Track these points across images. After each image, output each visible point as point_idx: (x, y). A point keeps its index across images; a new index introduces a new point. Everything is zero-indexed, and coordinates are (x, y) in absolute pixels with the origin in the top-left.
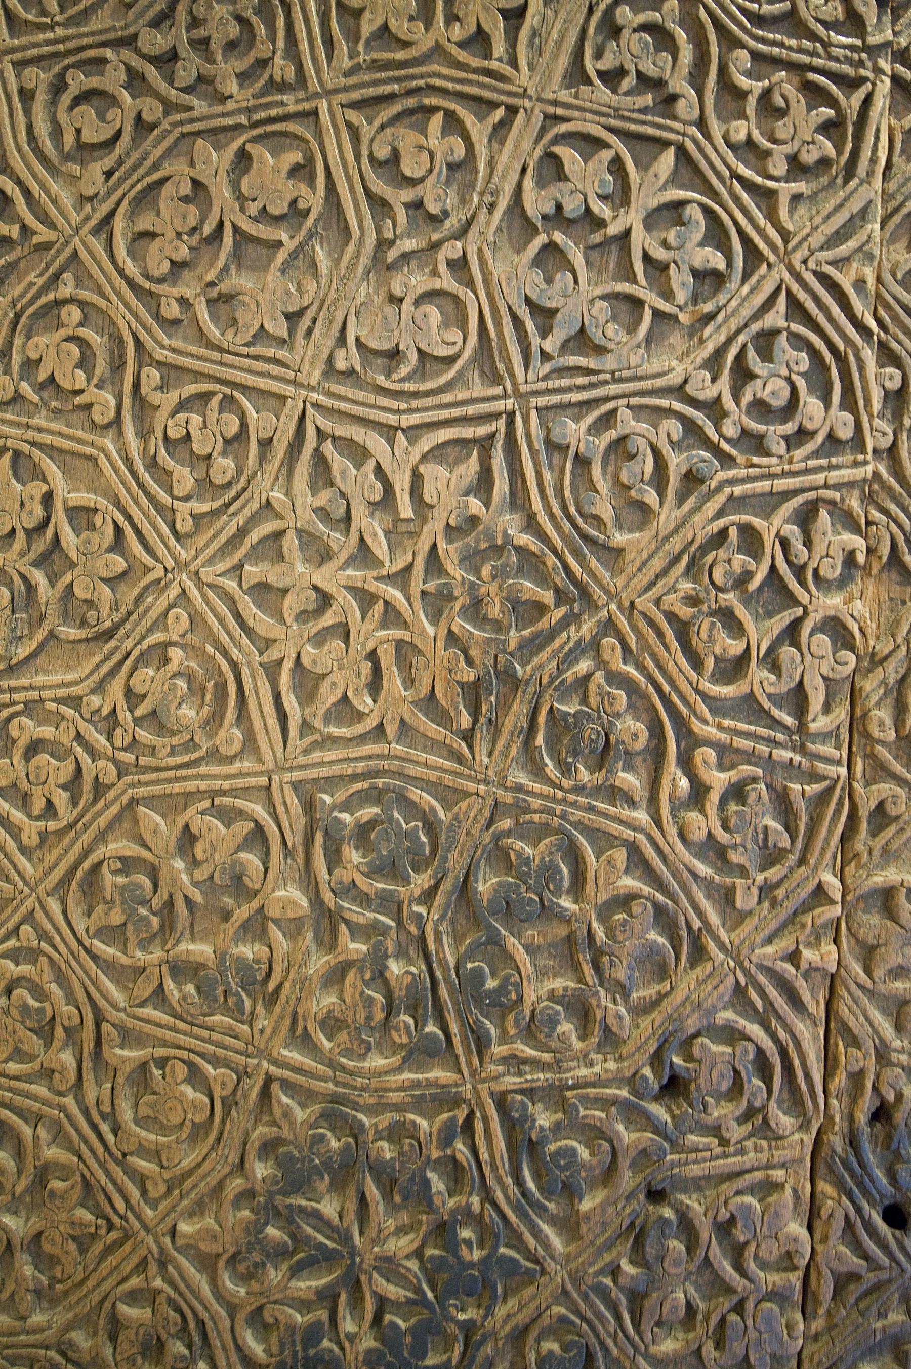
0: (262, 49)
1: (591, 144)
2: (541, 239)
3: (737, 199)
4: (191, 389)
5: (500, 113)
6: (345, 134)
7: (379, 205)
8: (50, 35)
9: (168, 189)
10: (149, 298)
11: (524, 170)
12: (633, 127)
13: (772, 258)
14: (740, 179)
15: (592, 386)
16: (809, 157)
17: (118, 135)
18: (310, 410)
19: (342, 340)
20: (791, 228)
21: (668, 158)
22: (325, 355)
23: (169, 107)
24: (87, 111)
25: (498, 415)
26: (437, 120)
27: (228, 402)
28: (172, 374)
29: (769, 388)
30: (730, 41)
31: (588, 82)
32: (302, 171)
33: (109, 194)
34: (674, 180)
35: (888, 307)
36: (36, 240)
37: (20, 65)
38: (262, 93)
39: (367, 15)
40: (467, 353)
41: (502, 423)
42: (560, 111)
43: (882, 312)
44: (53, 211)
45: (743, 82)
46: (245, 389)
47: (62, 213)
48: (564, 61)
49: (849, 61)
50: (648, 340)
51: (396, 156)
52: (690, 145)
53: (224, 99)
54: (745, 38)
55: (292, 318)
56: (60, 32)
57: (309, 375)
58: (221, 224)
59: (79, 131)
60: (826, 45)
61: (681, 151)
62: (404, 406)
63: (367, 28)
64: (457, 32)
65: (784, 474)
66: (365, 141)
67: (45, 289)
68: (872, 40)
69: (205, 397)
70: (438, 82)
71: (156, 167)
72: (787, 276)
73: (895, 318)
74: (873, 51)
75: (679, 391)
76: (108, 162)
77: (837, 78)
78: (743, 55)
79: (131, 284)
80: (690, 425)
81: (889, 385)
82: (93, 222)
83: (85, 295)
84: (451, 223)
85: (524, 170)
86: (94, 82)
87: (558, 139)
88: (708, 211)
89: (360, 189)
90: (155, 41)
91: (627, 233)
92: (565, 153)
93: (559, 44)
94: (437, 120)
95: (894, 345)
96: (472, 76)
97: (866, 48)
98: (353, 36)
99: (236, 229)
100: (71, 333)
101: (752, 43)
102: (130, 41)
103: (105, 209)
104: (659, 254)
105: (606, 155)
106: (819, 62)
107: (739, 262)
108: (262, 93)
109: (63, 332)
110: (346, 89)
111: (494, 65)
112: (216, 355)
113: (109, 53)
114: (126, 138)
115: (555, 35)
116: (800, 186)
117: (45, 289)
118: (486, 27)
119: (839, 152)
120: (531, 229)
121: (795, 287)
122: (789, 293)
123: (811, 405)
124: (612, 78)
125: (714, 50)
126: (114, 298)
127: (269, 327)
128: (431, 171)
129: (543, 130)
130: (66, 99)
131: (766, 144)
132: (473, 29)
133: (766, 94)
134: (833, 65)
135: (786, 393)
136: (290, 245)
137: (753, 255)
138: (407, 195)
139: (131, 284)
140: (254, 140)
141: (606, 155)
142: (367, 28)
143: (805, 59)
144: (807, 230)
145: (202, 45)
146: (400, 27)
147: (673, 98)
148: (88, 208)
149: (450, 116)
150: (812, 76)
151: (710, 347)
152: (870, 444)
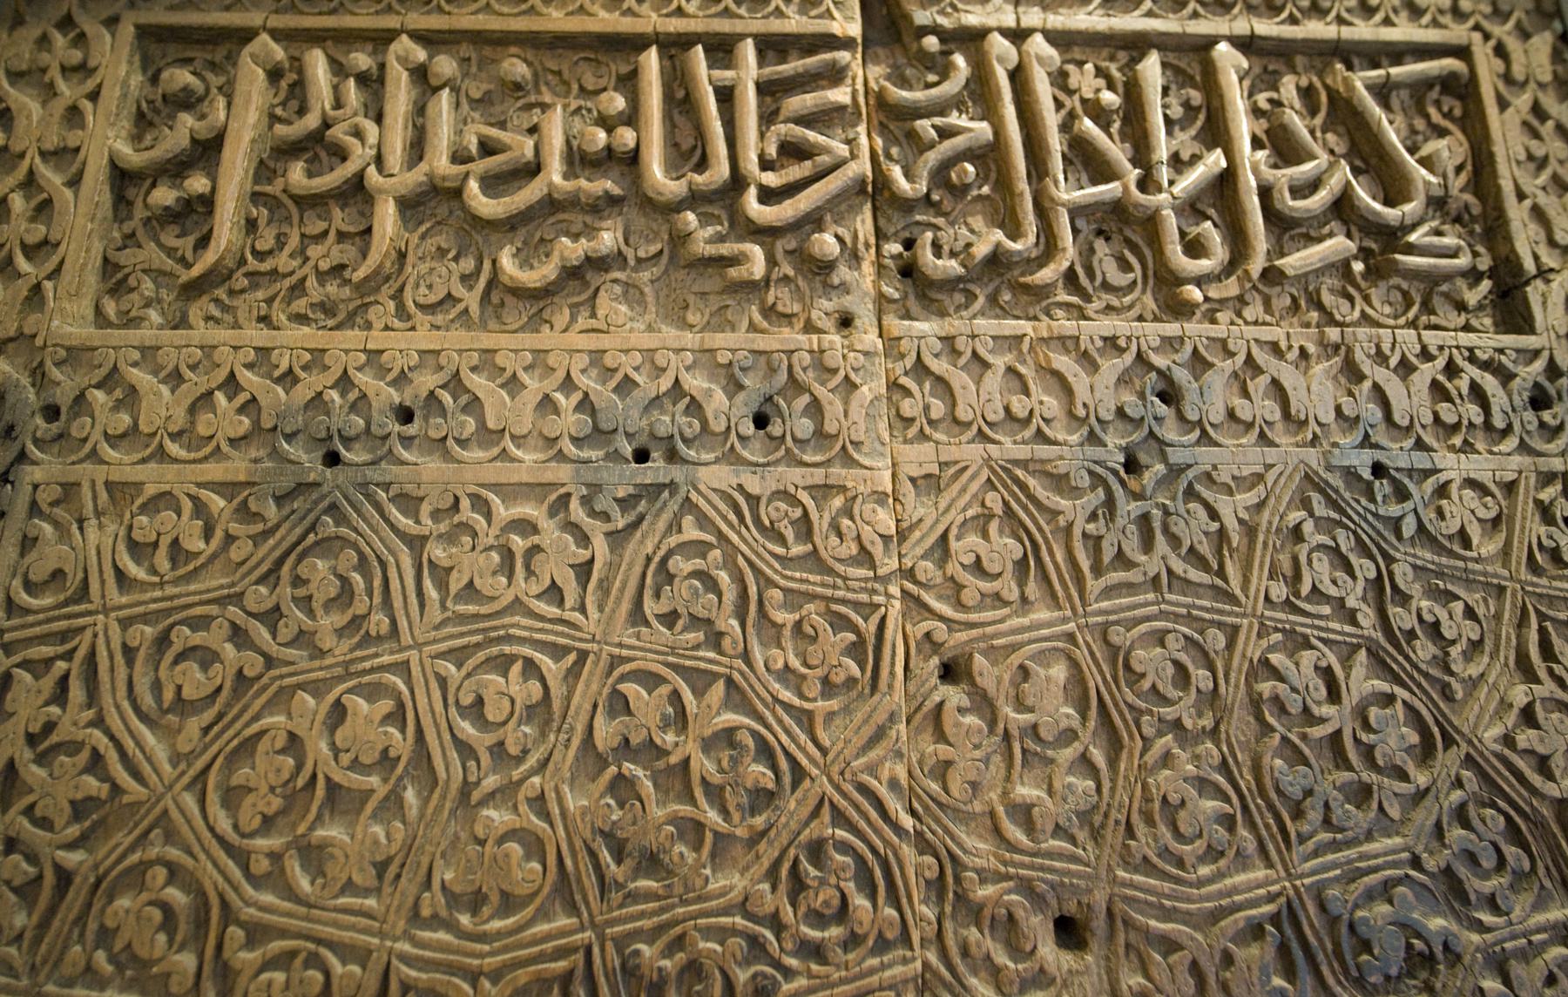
0: (360, 607)
1: (651, 680)
2: (613, 769)
3: (780, 722)
4: (277, 946)
5: (572, 657)
6: (434, 685)
7: (466, 750)
8: (158, 594)
9: (263, 746)
10: (242, 858)
11: (595, 706)
12: (688, 663)
13: (815, 771)
14: (782, 703)
15: (663, 910)
16: (839, 678)
17: (219, 689)
18: (395, 962)
19: (428, 884)
20: (827, 743)
21: (720, 687)
22: (411, 900)
23: (270, 662)
24: (192, 667)
25: (576, 950)
26: (517, 668)
27: (314, 961)
28: (256, 934)
29: (821, 898)
30: (766, 582)
31: (647, 624)
32: (397, 717)
33: (205, 749)
34: (727, 704)
35: (919, 798)
36: (126, 799)
37: (125, 623)
38: (359, 646)
39: (454, 574)
40: (546, 890)
41: (579, 957)
42: (625, 652)
43: (916, 805)
44: (146, 769)
45: (780, 616)
46: (330, 944)
47: (156, 770)
48: (626, 606)
49: (865, 590)
50: (713, 855)
51: (480, 701)
52: (736, 676)
53: (322, 653)
54: (777, 578)
55: (381, 867)
56: (170, 590)
57: (394, 926)
58: (314, 776)
59: (179, 688)
60: (845, 579)
61: (730, 682)
62: (487, 948)
63: (456, 584)
64: (535, 589)
65: (842, 981)
66: (451, 691)
67: (132, 849)
68: (880, 572)
69: (293, 954)
70: (518, 632)
71: (256, 718)
72: (830, 789)
73: (926, 808)
74: (885, 580)
75: (743, 906)
76: (209, 716)
77: (856, 605)
78: (777, 594)
79: (221, 840)
80: (755, 942)
81: (928, 874)
82: (186, 779)
83: (174, 853)
84: (532, 761)
85: (595, 706)
86: (198, 638)
87: (623, 678)
88: (755, 734)
89: (447, 737)
90: (259, 597)
91: (687, 761)
92: (629, 688)
93: (622, 590)
94: (517, 668)
95: (929, 835)
96: (548, 626)
97: (876, 578)
98: (442, 586)
99: (328, 779)
100: (153, 897)
101: (782, 582)
102: (237, 599)
103: (200, 764)
104: (717, 779)
105: (664, 690)
106: (840, 593)
107: (787, 779)
108: (359, 646)
109: (145, 896)
110: (435, 641)
111: (567, 615)
112: (303, 910)
113: (213, 610)
114: (225, 693)
115: (617, 584)
116: (834, 704)
117: (132, 849)
118: (559, 582)
119: (863, 670)
120: (603, 763)
121: (837, 798)
122: (831, 802)
123: (860, 902)
124: (670, 619)
125: (753, 590)
126: (202, 856)
127: (357, 878)
128: (512, 713)
129: (612, 668)
130: (169, 656)
131: (803, 670)
132: (548, 582)
133: (798, 625)
134: (850, 596)
135: (836, 902)
136: (382, 791)
137: (799, 773)
138: (490, 739)
139: (221, 840)
140: (349, 691)
141: (664, 690)
142: (456, 584)
143: (829, 592)
144: (840, 745)
145: (306, 603)
146: (483, 584)
147: (720, 635)
148: (183, 766)
149: (529, 664)
150: (835, 607)
151: (766, 863)
152: (916, 937)
